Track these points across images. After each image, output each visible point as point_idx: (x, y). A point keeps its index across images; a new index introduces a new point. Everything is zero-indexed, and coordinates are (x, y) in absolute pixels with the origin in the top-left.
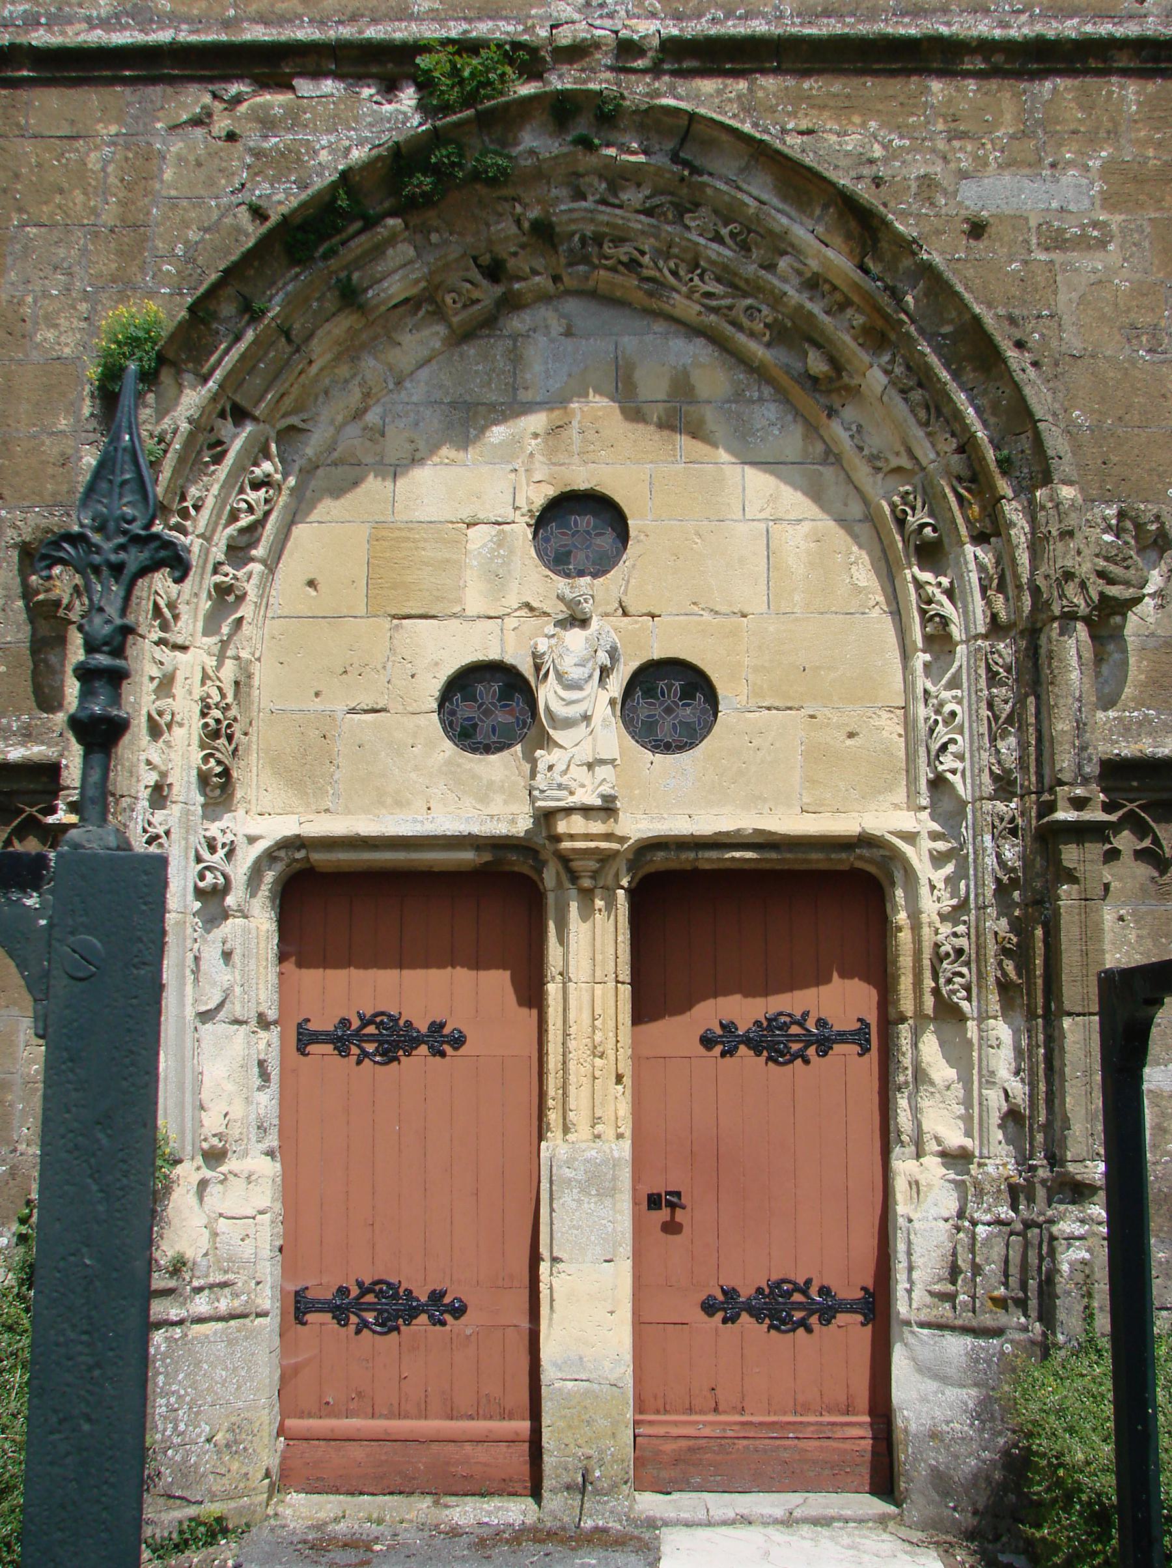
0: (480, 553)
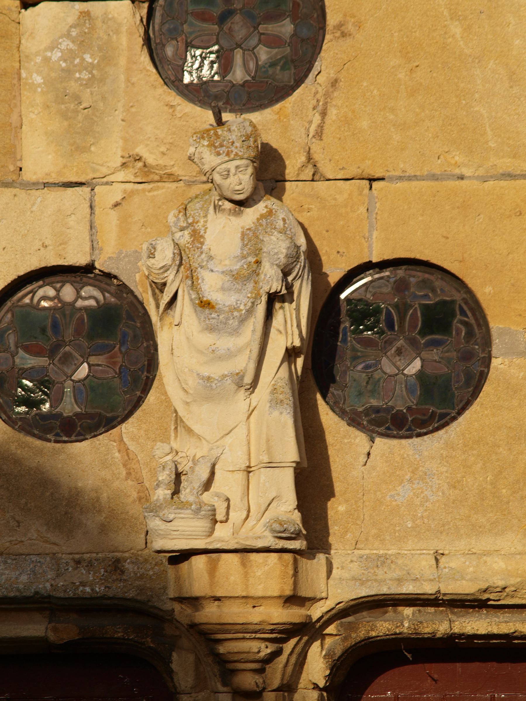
0: (47, 60)
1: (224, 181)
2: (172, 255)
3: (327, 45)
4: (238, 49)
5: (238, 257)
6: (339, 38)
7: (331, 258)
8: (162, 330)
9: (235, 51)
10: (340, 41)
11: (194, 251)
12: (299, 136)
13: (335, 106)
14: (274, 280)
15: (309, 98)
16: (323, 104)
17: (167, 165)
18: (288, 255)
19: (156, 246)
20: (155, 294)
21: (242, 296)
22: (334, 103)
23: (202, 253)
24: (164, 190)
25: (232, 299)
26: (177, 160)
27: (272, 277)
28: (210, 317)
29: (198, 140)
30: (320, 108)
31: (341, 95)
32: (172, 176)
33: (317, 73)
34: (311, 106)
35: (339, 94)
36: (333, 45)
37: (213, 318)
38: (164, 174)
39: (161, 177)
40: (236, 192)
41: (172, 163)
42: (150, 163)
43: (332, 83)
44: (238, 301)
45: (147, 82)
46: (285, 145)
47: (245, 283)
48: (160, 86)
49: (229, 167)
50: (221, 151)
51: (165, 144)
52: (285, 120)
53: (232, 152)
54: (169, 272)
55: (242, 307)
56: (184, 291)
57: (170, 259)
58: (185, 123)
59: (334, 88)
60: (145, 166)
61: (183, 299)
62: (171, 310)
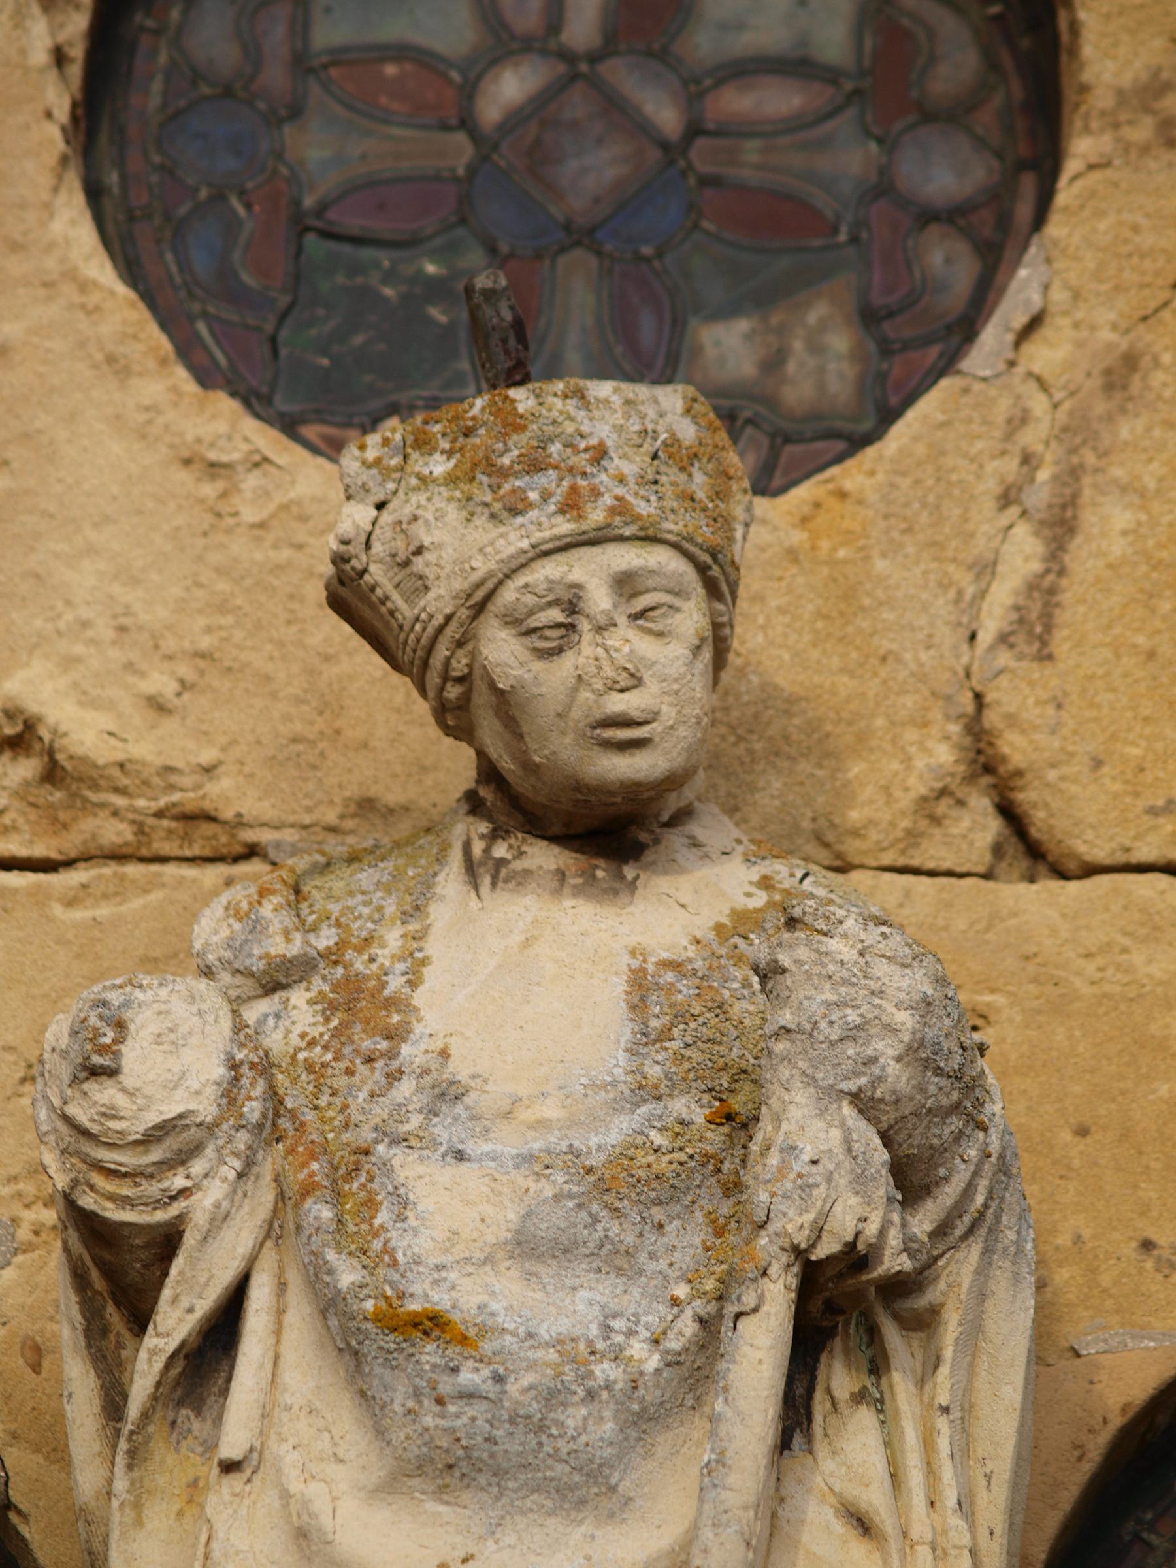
1: (538, 666)
2: (220, 1071)
3: (1079, 184)
4: (578, 253)
5: (614, 1084)
6: (1145, 150)
7: (1105, 1280)
8: (139, 1523)
9: (562, 261)
10: (1153, 165)
11: (350, 1072)
12: (920, 636)
13: (1124, 489)
14: (842, 1181)
15: (980, 445)
16: (1055, 478)
17: (179, 764)
18: (922, 1044)
19: (127, 1015)
20: (105, 1331)
21: (636, 1292)
22: (1117, 472)
23: (394, 1076)
24: (155, 896)
25: (581, 1307)
26: (233, 742)
27: (827, 1164)
28: (446, 1386)
29: (395, 461)
30: (1040, 494)
31: (1157, 432)
32: (207, 828)
33: (1020, 320)
34: (990, 486)
35: (1149, 429)
36: (1116, 185)
37: (468, 1396)
38: (159, 814)
39: (140, 829)
40: (609, 733)
41: (207, 756)
42: (79, 751)
43: (1108, 372)
44: (615, 1316)
45: (82, 345)
46: (845, 679)
47: (658, 1214)
48: (151, 364)
49: (576, 576)
50: (533, 487)
51: (170, 658)
52: (842, 553)
53: (596, 493)
54: (198, 1167)
55: (638, 1348)
56: (282, 1287)
57: (211, 1092)
58: (286, 554)
59: (1118, 395)
60: (53, 774)
61: (278, 1332)
62: (198, 1413)
